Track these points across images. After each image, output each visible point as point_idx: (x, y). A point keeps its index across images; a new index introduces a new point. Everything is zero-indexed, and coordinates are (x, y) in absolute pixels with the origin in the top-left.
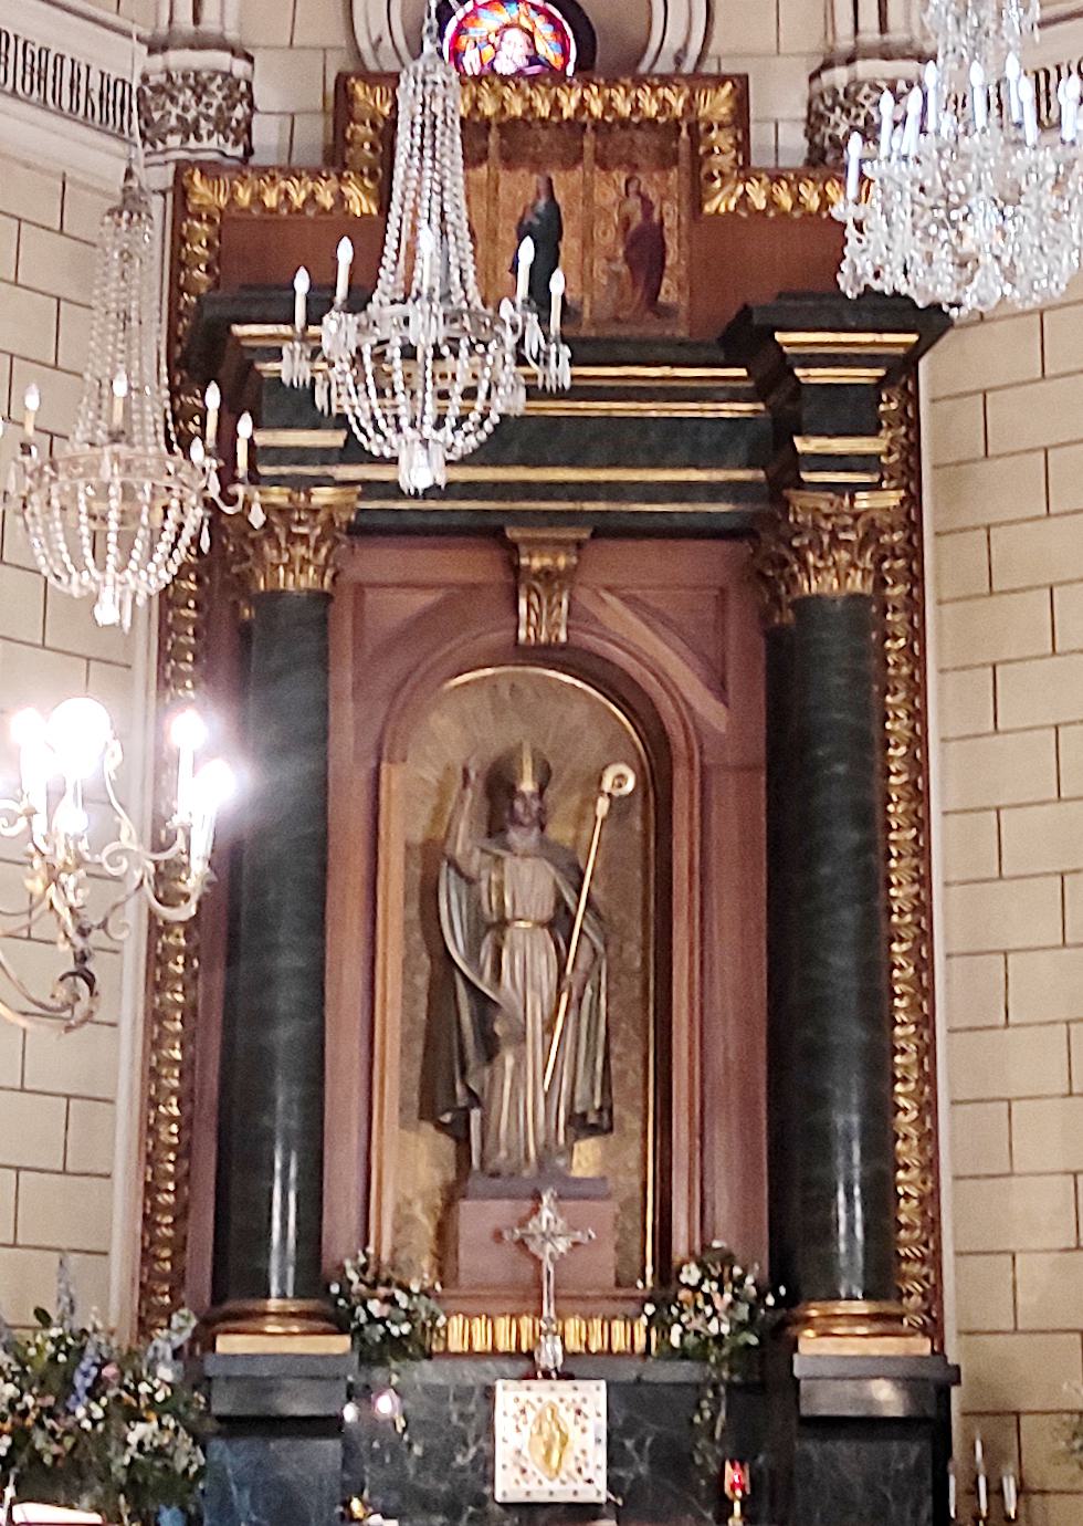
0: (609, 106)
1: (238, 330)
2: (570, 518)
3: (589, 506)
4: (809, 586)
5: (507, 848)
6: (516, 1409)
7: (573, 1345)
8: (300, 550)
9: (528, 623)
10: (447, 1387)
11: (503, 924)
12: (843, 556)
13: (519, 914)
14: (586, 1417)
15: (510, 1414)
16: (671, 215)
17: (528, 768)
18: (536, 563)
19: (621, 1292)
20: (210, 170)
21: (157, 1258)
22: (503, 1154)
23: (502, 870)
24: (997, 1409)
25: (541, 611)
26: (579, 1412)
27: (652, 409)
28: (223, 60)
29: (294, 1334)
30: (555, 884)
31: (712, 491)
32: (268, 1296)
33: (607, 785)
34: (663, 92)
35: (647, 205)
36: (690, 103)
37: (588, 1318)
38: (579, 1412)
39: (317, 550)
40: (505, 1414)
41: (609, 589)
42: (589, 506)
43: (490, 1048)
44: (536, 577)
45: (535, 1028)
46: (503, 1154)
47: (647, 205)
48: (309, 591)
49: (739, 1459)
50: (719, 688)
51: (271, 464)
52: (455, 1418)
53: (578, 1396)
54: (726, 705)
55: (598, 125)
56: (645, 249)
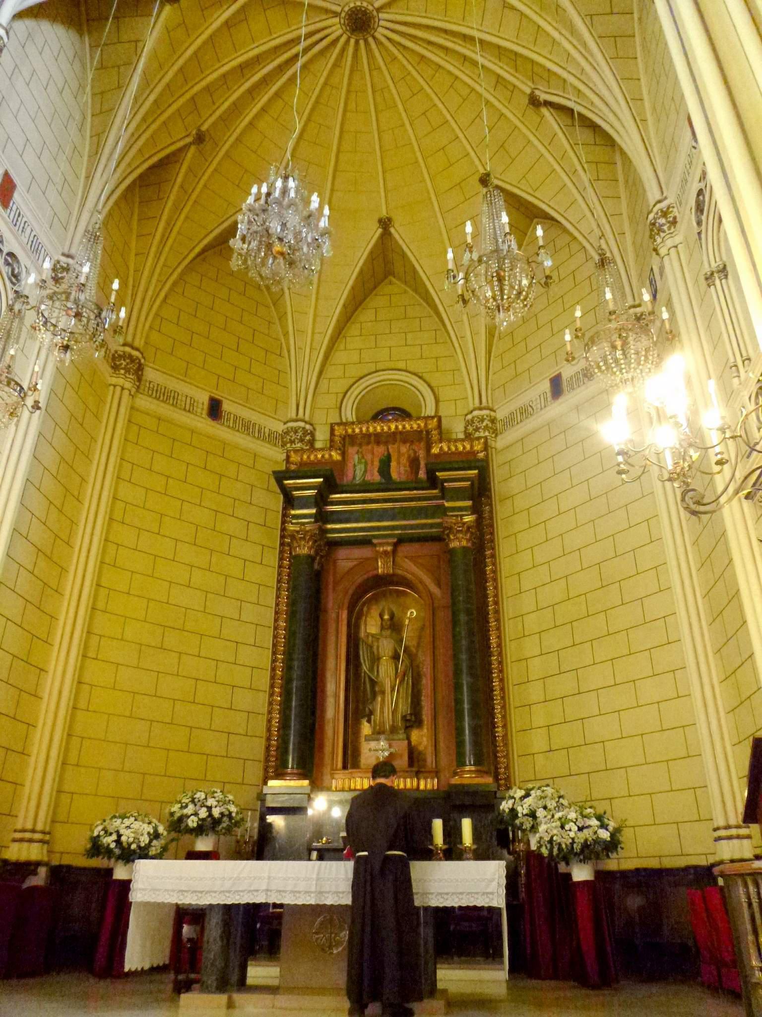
0: (404, 427)
1: (286, 482)
8: (303, 543)
11: (379, 659)
16: (422, 454)
17: (386, 612)
18: (381, 549)
20: (296, 451)
21: (269, 761)
27: (413, 504)
28: (302, 424)
31: (432, 526)
32: (288, 768)
34: (419, 422)
35: (415, 452)
36: (426, 424)
41: (406, 557)
43: (374, 695)
45: (388, 689)
47: (415, 452)
49: (722, 888)
50: (439, 585)
55: (401, 433)
56: (414, 463)
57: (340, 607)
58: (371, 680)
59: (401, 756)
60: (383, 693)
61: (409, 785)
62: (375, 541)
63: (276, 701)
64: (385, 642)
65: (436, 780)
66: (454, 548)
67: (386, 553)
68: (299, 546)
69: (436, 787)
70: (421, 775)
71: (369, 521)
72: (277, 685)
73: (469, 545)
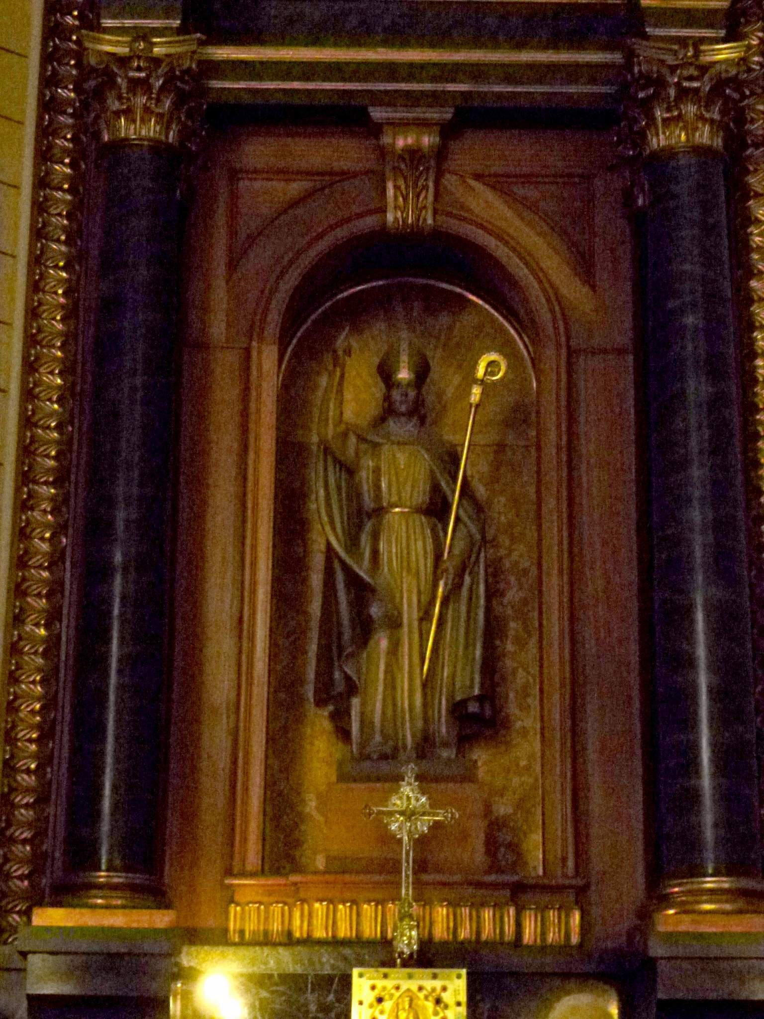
2: (436, 99)
3: (451, 87)
4: (659, 140)
5: (387, 436)
6: (371, 997)
7: (440, 932)
8: (141, 100)
9: (396, 207)
10: (307, 975)
11: (379, 511)
12: (690, 109)
13: (394, 499)
14: (446, 1007)
15: (366, 1004)
17: (404, 358)
18: (400, 143)
19: (492, 878)
22: (378, 738)
23: (379, 459)
24: (236, 686)
25: (408, 194)
26: (438, 1001)
29: (116, 907)
30: (432, 471)
33: (480, 372)
37: (454, 904)
38: (438, 1001)
39: (158, 100)
40: (361, 1003)
41: (478, 177)
42: (451, 87)
44: (401, 158)
45: (410, 613)
46: (378, 738)
48: (150, 140)
51: (114, 17)
52: (313, 1008)
53: (438, 984)
54: (593, 287)
57: (255, 330)
58: (353, 580)
59: (464, 836)
60: (394, 623)
61: (488, 931)
62: (377, 114)
63: (32, 638)
64: (402, 458)
65: (576, 917)
66: (670, 153)
67: (413, 155)
68: (128, 112)
69: (575, 939)
70: (524, 898)
71: (356, 41)
72: (34, 589)
73: (718, 142)
